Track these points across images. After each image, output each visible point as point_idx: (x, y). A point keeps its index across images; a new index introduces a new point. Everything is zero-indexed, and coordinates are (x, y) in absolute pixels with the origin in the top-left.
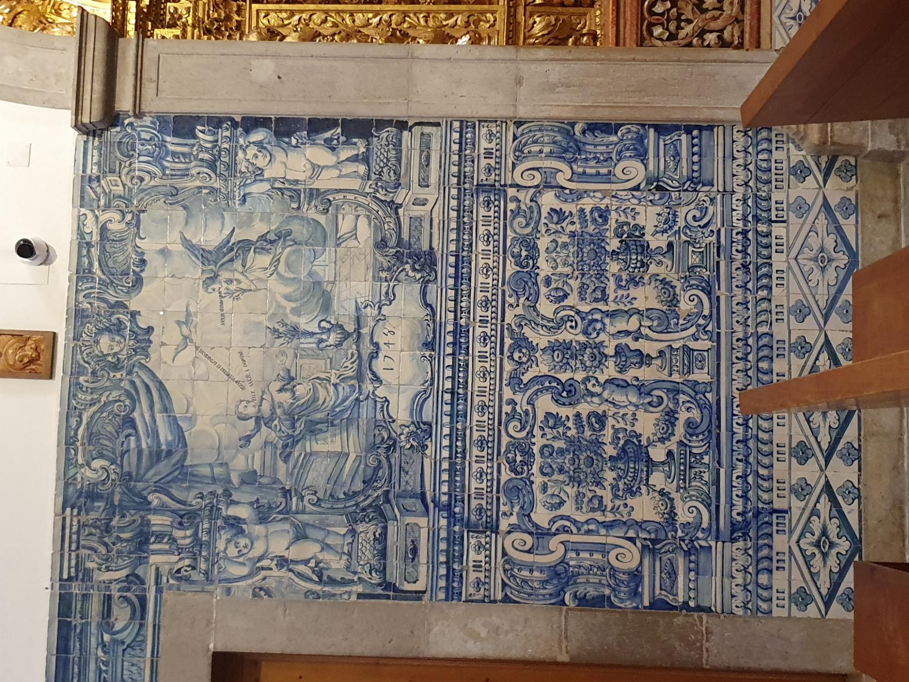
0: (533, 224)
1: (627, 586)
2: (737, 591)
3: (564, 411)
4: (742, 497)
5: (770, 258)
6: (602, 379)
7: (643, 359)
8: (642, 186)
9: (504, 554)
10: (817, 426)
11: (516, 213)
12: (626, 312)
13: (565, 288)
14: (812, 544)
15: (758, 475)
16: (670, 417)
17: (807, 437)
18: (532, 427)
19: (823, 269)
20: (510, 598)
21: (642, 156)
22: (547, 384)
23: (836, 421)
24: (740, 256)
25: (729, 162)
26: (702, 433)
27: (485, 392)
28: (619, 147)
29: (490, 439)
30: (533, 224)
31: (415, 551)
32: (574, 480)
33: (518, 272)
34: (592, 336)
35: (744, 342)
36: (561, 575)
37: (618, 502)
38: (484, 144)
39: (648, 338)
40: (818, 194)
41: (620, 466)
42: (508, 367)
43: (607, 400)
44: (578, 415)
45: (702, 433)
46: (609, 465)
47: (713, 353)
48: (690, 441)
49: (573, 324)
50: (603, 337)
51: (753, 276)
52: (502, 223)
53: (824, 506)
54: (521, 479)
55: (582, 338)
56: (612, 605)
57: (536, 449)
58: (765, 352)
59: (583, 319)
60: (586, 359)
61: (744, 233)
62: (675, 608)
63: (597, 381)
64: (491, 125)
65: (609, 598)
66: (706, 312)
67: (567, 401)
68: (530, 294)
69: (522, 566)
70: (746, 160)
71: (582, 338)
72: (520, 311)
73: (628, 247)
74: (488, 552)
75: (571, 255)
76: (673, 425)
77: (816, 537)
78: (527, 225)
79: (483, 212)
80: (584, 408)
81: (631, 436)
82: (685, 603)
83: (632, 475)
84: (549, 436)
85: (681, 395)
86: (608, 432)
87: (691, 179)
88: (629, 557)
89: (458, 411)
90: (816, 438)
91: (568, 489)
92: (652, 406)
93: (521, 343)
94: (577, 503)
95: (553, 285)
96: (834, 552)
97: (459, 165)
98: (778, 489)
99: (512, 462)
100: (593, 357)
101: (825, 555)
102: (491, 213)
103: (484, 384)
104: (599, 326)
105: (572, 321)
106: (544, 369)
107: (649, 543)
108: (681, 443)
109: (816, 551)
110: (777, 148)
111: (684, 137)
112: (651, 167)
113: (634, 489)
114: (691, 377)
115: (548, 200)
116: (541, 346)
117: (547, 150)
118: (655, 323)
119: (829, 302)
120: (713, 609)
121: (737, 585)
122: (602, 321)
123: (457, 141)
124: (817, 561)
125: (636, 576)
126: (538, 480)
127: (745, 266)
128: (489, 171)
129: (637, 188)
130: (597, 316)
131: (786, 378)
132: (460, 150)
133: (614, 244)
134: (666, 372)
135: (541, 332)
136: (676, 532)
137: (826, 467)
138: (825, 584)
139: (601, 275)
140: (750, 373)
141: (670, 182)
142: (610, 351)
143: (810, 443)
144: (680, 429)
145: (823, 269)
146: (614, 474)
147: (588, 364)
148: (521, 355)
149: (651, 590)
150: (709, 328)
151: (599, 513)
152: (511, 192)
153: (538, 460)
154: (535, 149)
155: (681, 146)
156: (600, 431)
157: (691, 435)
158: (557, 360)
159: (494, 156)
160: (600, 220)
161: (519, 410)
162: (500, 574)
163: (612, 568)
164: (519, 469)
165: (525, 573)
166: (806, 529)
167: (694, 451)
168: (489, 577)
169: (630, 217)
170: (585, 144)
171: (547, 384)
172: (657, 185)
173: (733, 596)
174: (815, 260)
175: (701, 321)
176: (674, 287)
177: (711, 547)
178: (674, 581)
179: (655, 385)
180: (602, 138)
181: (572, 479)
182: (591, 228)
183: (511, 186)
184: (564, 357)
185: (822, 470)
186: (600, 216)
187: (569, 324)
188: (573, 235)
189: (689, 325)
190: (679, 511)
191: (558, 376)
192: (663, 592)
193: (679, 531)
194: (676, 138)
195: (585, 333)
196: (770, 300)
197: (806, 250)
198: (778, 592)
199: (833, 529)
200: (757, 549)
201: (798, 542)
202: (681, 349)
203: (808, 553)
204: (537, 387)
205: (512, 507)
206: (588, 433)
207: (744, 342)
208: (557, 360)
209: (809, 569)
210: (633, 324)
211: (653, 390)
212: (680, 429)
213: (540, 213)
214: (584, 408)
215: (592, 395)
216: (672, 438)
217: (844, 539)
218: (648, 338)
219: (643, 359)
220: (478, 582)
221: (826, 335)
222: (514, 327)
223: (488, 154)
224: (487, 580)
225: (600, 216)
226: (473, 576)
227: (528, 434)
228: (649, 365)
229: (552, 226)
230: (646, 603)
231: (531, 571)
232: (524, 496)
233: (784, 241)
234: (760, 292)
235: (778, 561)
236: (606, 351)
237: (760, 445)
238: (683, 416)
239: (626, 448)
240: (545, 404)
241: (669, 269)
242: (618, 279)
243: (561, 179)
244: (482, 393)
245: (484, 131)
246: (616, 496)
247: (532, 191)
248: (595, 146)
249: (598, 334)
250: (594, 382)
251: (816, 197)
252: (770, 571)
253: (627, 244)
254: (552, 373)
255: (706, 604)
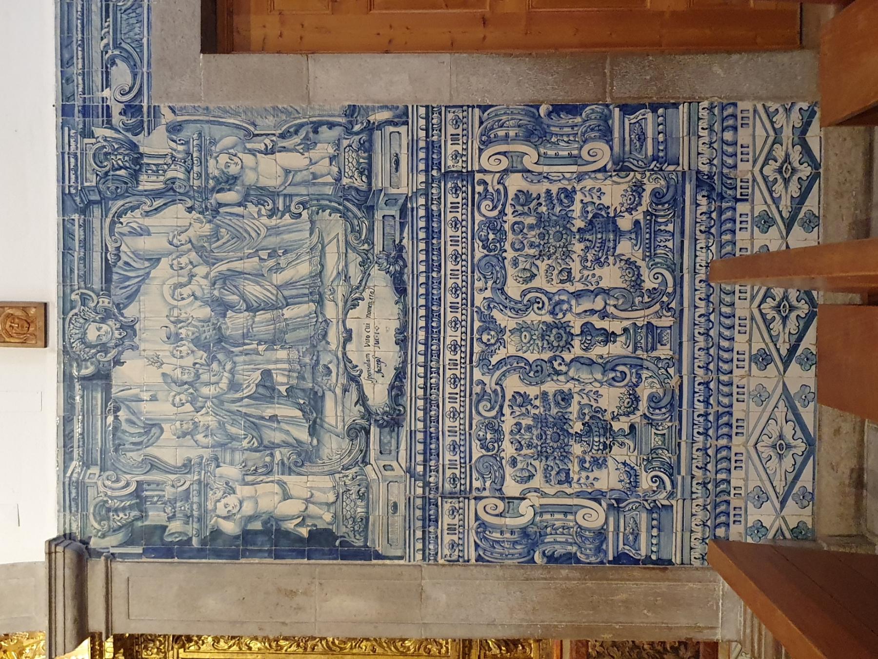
0: (497, 408)
1: (592, 543)
2: (702, 148)
3: (533, 391)
4: (703, 402)
5: (731, 406)
6: (568, 357)
7: (609, 337)
8: (608, 167)
9: (477, 518)
10: (778, 195)
11: (485, 195)
12: (592, 292)
13: (530, 468)
14: (773, 308)
15: (719, 348)
16: (638, 189)
17: (767, 344)
18: (504, 205)
19: (781, 457)
20: (483, 558)
21: (606, 134)
22: (515, 364)
23: (797, 190)
24: (701, 438)
25: (687, 535)
26: (665, 407)
27: (458, 241)
28: (583, 129)
29: (463, 376)
30: (499, 208)
31: (397, 163)
32: (541, 454)
33: (487, 256)
34: (558, 317)
35: (706, 318)
36: (530, 537)
37: (586, 273)
38: (451, 130)
39: (615, 317)
40: (778, 382)
41: (587, 237)
42: (477, 348)
43: (573, 379)
44: (548, 192)
45: (665, 407)
46: (577, 237)
47: (676, 329)
48: (652, 414)
49: (540, 305)
50: (569, 317)
51: (718, 118)
52: (469, 209)
53: (781, 412)
54: (491, 456)
55: (549, 319)
56: (578, 561)
57: (507, 227)
58: (723, 519)
59: (550, 299)
60: (552, 338)
61: (706, 384)
62: (637, 562)
63: (563, 360)
64: (454, 500)
65: (575, 553)
66: (670, 290)
67: (533, 380)
68: (498, 278)
69: (494, 528)
70: (706, 444)
71: (549, 319)
72: (488, 294)
73: (591, 430)
74: (461, 517)
75: (534, 438)
76: (640, 197)
77: (778, 164)
78: (495, 208)
79: (451, 198)
80: (550, 387)
81: (600, 209)
82: (648, 557)
83: (599, 245)
84: (518, 413)
85: (645, 371)
86: (577, 207)
87: (655, 158)
88: (594, 516)
89: (430, 515)
90: (775, 345)
91: (536, 463)
92: (615, 381)
93: (489, 324)
94: (546, 477)
95: (521, 266)
96: (793, 315)
97: (425, 377)
98: (740, 292)
99: (482, 441)
100: (559, 337)
101: (786, 181)
102: (459, 200)
103: (456, 200)
104: (565, 307)
105: (539, 303)
106: (512, 350)
107: (613, 501)
108: (647, 213)
109: (778, 177)
110: (734, 522)
111: (650, 116)
112: (616, 149)
113: (602, 260)
114: (655, 354)
115: (515, 183)
116: (509, 328)
117: (512, 133)
118: (621, 302)
119: (786, 488)
120: (673, 560)
121: (703, 109)
122: (568, 302)
123: (423, 341)
124: (779, 188)
125: (601, 534)
126: (510, 254)
127: (707, 299)
128: (453, 546)
129: (603, 170)
130: (564, 297)
131: (749, 253)
132: (425, 461)
133: (578, 427)
134: (630, 348)
135: (510, 314)
136: (643, 297)
137: (785, 372)
138: (785, 204)
139: (566, 455)
140: (715, 146)
141: (635, 162)
142: (577, 330)
143: (769, 350)
144: (646, 198)
145: (781, 457)
146: (582, 246)
147: (555, 344)
148: (490, 337)
149: (615, 545)
150: (673, 305)
151: (566, 485)
152: (478, 177)
153: (510, 236)
154: (501, 133)
155: (646, 124)
156: (569, 206)
157: (657, 205)
158: (525, 341)
159: (457, 532)
160: (563, 403)
161: (489, 391)
162: (473, 537)
163: (580, 527)
164: (490, 447)
165: (496, 535)
166: (769, 157)
167: (659, 220)
168: (467, 149)
169: (595, 197)
170: (549, 126)
171: (515, 364)
172: (621, 166)
173: (693, 515)
174: (774, 446)
175: (665, 299)
176: (638, 268)
177: (672, 506)
178: (636, 537)
179: (617, 362)
180: (566, 119)
181: (540, 454)
182: (554, 411)
183: (478, 172)
184: (531, 338)
185: (782, 237)
186: (563, 400)
187: (536, 306)
188: (535, 418)
189: (652, 303)
190: (645, 277)
191: (525, 356)
192: (627, 547)
193: (646, 297)
194: (641, 117)
195: (552, 313)
196: (730, 448)
197: (765, 438)
198: (738, 387)
199: (796, 155)
200: (716, 505)
201: (759, 306)
202: (645, 328)
203: (771, 179)
204: (505, 368)
205: (485, 482)
206: (558, 208)
207: (706, 318)
208: (525, 341)
209: (769, 332)
210: (599, 304)
211: (617, 365)
212: (646, 198)
213: (503, 396)
214: (550, 387)
215: (558, 373)
216: (636, 412)
217: (803, 301)
218: (615, 317)
219: (609, 337)
220: (453, 545)
221: (784, 384)
222: (483, 310)
223: (451, 529)
224: (461, 542)
225: (563, 400)
226: (447, 539)
227: (500, 213)
228: (614, 342)
229: (519, 208)
230: (611, 558)
231: (502, 533)
232: (497, 272)
233: (750, 150)
234: (723, 237)
235: (741, 222)
236: (572, 331)
237: (722, 319)
238: (649, 187)
239: (594, 220)
240: (513, 384)
241: (632, 450)
242: (582, 461)
243: (529, 162)
244: (452, 466)
245: (450, 116)
246: (583, 468)
247: (498, 175)
248: (561, 127)
249: (564, 315)
250: (559, 361)
251: (776, 386)
252: (735, 129)
253: (589, 426)
254: (520, 354)
255: (665, 557)
